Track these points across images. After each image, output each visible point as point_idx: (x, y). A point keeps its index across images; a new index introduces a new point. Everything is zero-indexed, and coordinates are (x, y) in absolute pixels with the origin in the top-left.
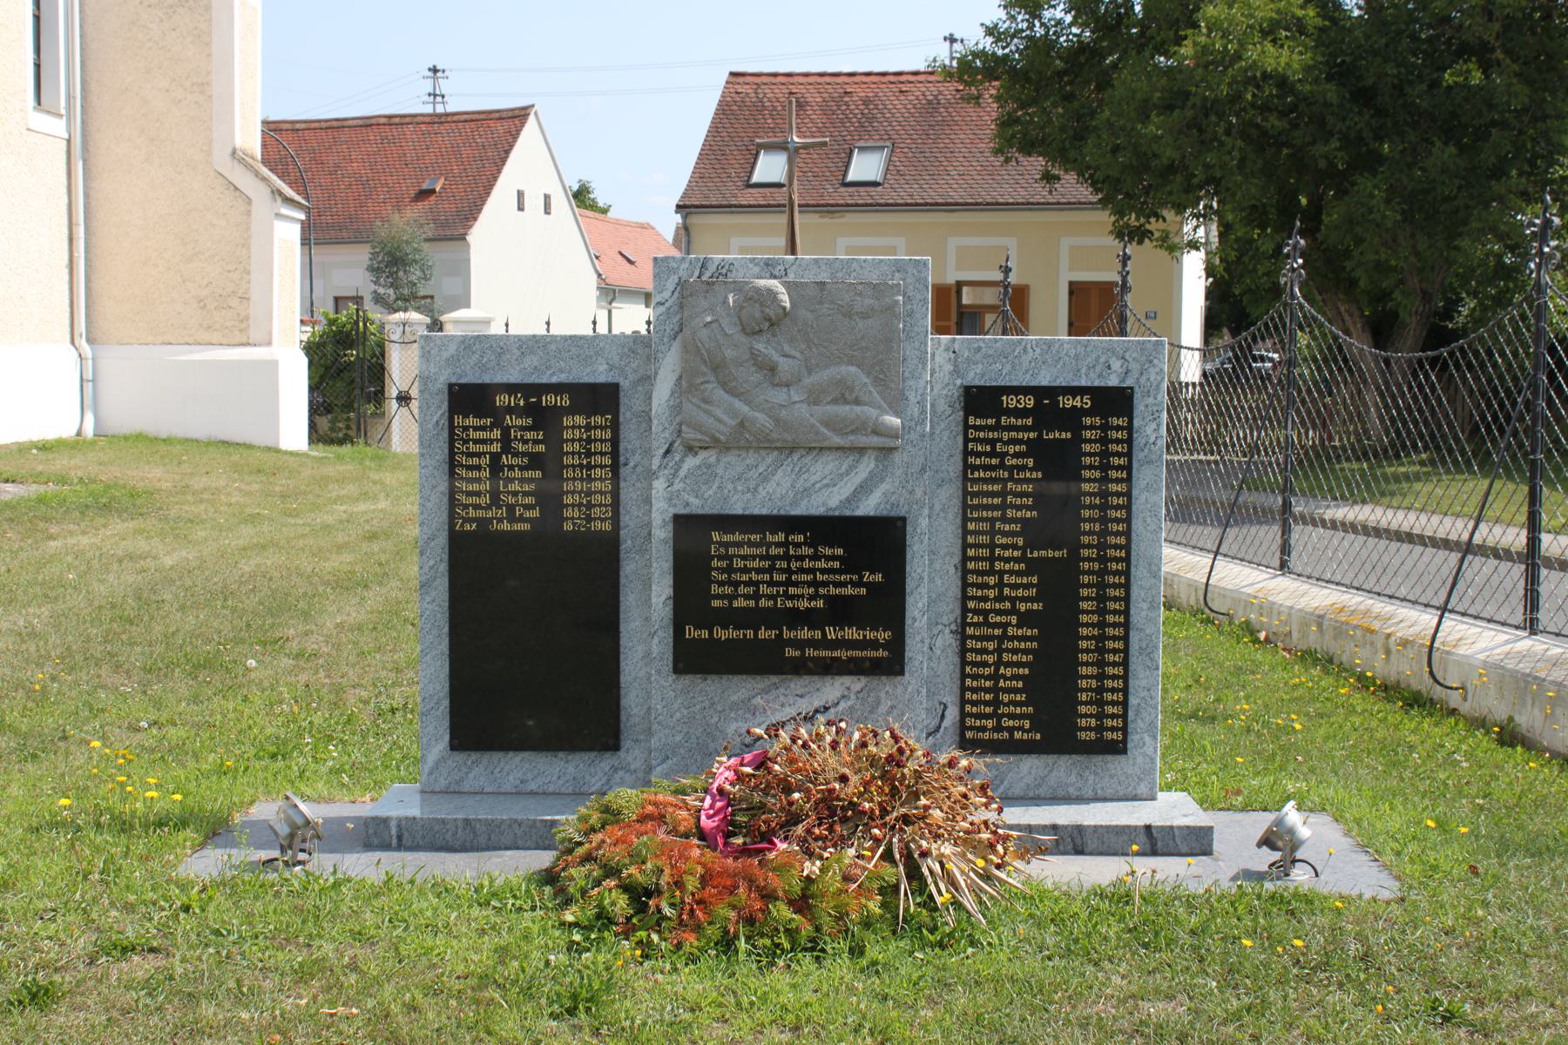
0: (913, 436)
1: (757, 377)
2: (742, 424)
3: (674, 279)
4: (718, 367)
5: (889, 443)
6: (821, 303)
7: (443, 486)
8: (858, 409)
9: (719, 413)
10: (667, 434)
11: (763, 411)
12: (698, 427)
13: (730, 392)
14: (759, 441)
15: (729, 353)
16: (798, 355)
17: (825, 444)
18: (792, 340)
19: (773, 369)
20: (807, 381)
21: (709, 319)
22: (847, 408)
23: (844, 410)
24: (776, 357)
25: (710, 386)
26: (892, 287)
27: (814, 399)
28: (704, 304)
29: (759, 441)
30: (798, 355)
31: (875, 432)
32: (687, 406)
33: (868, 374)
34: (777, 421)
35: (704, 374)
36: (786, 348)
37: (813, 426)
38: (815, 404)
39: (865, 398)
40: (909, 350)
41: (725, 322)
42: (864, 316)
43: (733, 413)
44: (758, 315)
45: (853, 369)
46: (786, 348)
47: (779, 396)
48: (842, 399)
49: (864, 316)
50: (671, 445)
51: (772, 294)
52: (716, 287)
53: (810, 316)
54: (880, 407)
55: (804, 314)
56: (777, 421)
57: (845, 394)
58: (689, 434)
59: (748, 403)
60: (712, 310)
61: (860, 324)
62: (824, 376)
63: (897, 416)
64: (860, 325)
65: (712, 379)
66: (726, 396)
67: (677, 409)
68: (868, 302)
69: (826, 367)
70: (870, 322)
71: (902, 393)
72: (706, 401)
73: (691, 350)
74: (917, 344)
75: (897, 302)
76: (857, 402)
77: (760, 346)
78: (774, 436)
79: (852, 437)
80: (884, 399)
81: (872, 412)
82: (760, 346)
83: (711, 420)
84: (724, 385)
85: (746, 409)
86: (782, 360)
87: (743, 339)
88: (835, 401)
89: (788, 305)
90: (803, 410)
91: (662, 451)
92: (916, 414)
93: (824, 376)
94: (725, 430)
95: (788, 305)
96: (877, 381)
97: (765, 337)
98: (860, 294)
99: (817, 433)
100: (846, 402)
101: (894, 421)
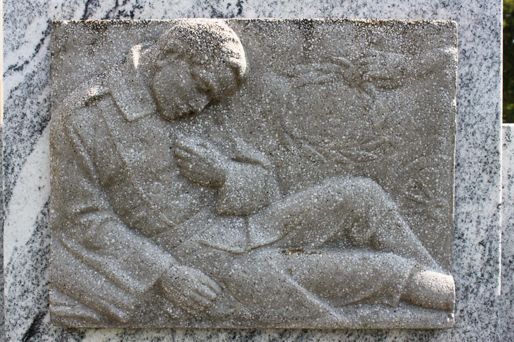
0: (473, 303)
1: (186, 200)
2: (158, 288)
3: (41, 24)
4: (111, 181)
5: (431, 319)
6: (306, 60)
7: (49, 195)
8: (376, 259)
9: (114, 267)
10: (29, 302)
11: (196, 264)
12: (77, 295)
13: (136, 227)
14: (190, 318)
15: (132, 155)
16: (262, 157)
17: (317, 323)
18: (251, 132)
19: (215, 185)
20: (281, 206)
21: (95, 91)
22: (356, 256)
23: (350, 261)
24: (221, 162)
25: (96, 218)
26: (439, 29)
27: (293, 240)
28: (88, 64)
29: (190, 318)
30: (262, 157)
31: (409, 301)
32: (59, 256)
33: (394, 193)
34: (224, 282)
35: (87, 196)
36: (242, 146)
37: (291, 292)
38: (297, 249)
39: (390, 239)
40: (465, 150)
41: (124, 97)
42: (387, 84)
43: (140, 267)
44: (184, 82)
45: (366, 184)
46: (242, 146)
47: (227, 236)
48: (346, 241)
49: (387, 84)
50: (38, 320)
51: (212, 42)
52: (111, 34)
53: (285, 86)
54: (415, 254)
55: (275, 82)
56: (224, 282)
57: (352, 232)
58: (63, 307)
59: (170, 248)
60: (100, 75)
61: (381, 100)
62: (309, 197)
63: (446, 266)
64: (380, 101)
65: (103, 203)
66: (128, 236)
67: (42, 257)
68: (394, 57)
69: (317, 180)
70: (397, 96)
71: (452, 224)
72: (91, 246)
73: (65, 152)
74: (479, 138)
75: (448, 57)
76: (374, 245)
77: (191, 142)
78: (221, 309)
79: (365, 311)
80: (423, 238)
81: (400, 264)
82: (191, 142)
83: (101, 282)
84: (124, 215)
85: (164, 260)
86: (233, 170)
87: (159, 129)
88: (332, 244)
89: (243, 63)
90: (272, 263)
91: (21, 331)
92: (478, 264)
93: (309, 197)
94: (127, 300)
95: (243, 63)
96: (410, 207)
97: (200, 125)
98: (379, 44)
99: (300, 304)
100: (352, 244)
101: (439, 279)
